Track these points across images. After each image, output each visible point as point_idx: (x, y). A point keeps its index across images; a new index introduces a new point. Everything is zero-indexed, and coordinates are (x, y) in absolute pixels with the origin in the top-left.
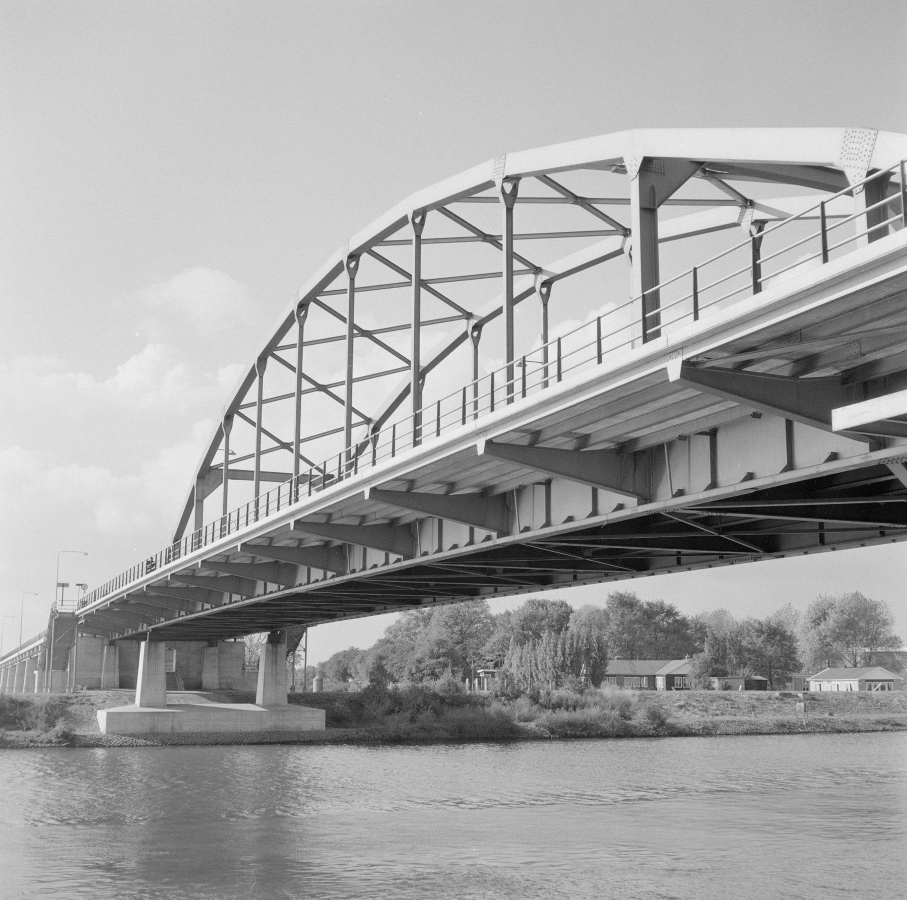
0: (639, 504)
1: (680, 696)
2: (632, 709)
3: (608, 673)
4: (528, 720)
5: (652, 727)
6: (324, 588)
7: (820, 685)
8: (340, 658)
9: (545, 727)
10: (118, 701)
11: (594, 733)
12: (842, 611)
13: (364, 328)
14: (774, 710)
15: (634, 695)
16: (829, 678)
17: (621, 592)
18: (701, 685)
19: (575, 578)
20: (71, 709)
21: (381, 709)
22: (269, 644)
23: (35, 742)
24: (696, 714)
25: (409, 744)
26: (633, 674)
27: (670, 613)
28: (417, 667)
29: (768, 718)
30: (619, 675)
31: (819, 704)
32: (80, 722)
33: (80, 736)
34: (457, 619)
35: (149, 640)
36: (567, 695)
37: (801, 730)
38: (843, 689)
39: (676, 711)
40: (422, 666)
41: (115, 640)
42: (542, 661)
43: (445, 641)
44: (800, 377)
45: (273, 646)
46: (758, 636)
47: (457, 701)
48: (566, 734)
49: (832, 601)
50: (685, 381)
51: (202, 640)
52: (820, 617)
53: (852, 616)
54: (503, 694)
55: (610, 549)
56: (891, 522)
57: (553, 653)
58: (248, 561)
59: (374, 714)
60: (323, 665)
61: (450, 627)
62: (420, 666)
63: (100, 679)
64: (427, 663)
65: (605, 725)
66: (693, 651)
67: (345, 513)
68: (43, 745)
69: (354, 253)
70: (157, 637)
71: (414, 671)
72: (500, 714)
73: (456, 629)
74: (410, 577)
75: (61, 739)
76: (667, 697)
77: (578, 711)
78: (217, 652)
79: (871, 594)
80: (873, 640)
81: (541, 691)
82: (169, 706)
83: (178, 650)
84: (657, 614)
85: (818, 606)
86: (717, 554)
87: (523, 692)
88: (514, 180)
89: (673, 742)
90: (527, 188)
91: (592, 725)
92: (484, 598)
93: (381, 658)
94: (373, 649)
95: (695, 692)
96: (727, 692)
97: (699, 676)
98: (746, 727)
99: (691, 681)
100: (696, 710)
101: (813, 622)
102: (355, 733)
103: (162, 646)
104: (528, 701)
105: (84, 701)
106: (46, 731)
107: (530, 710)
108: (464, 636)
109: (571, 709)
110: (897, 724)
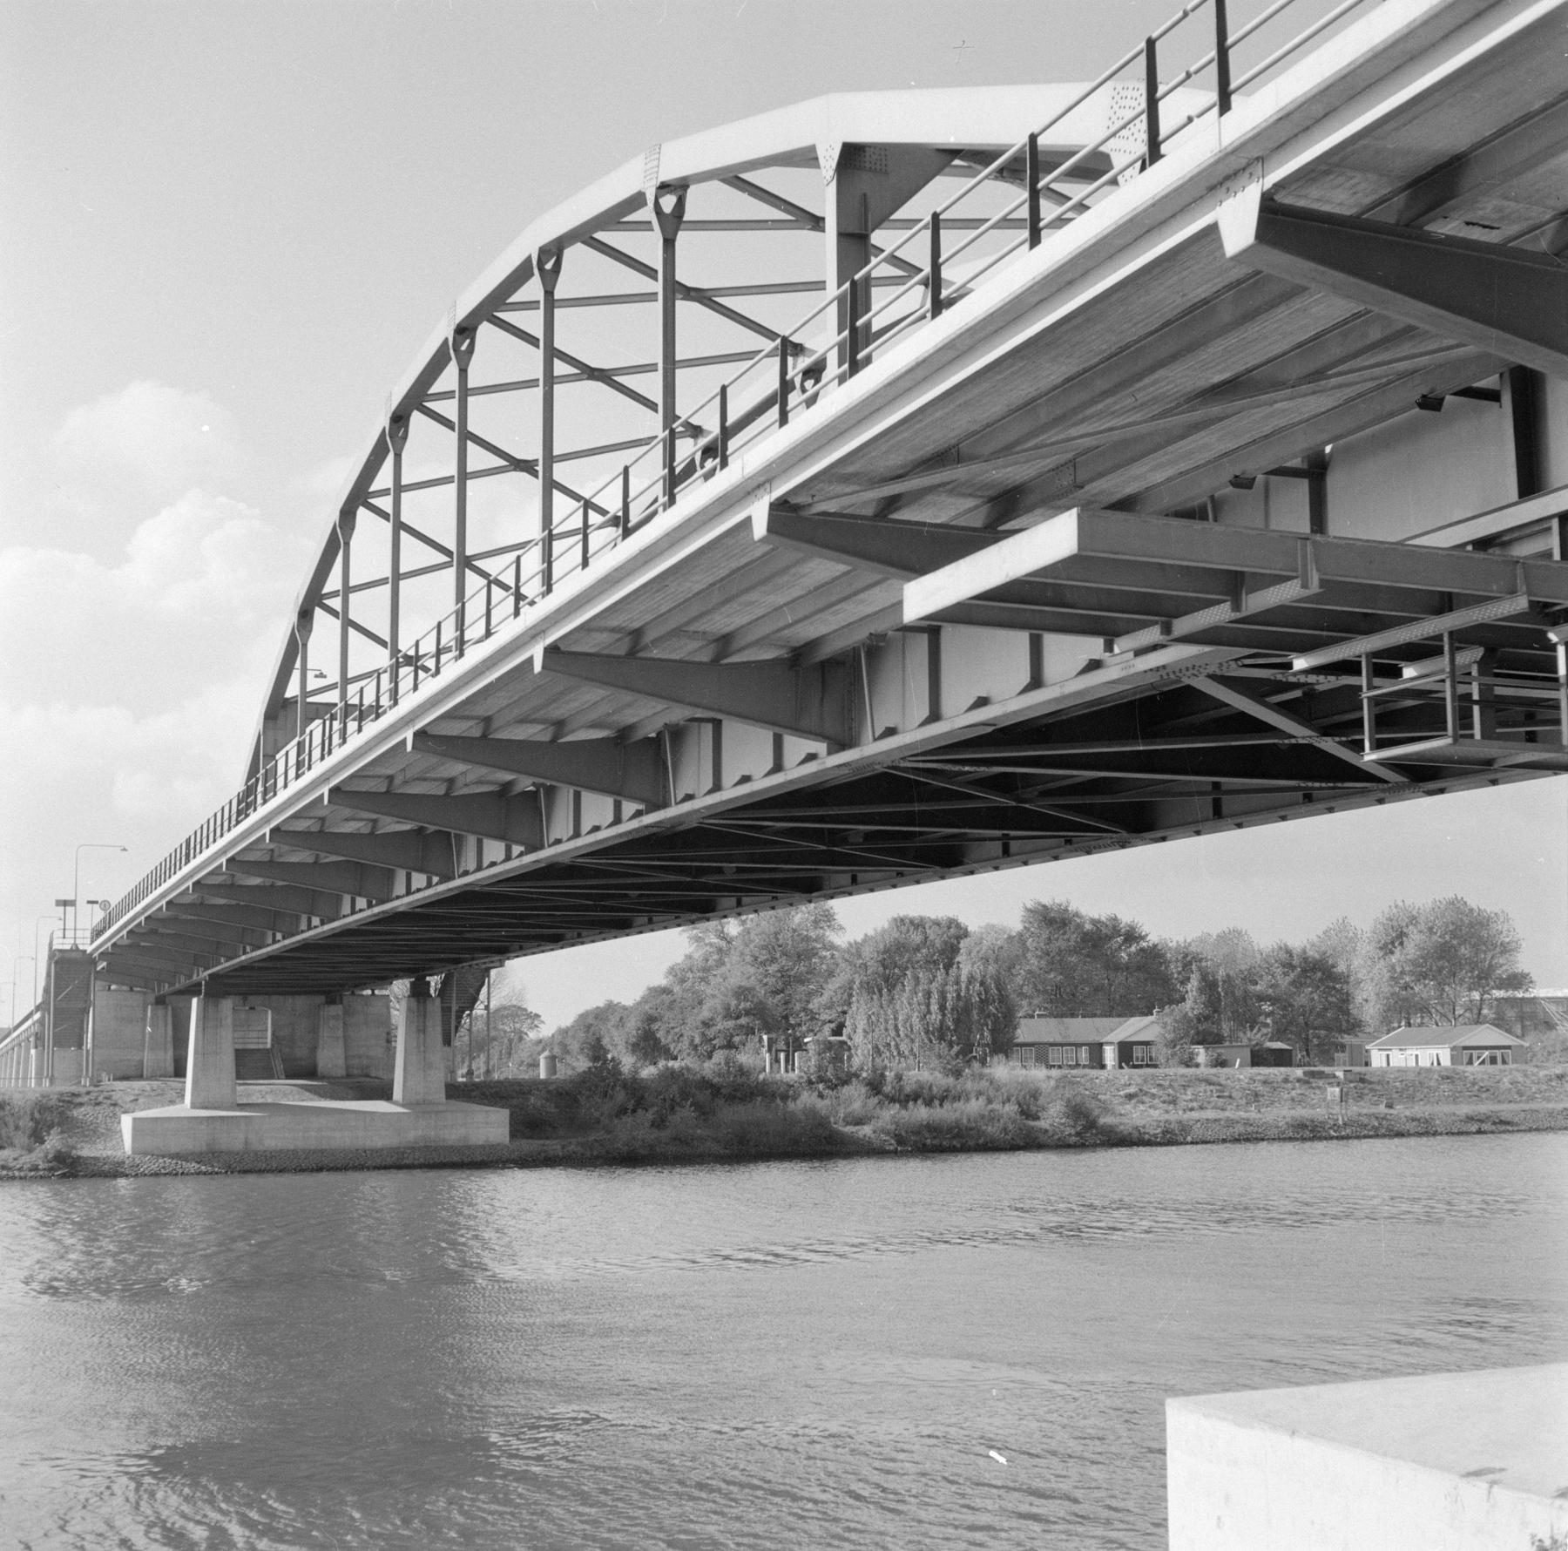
0: (830, 753)
1: (1130, 1078)
2: (1041, 1101)
3: (1020, 1040)
4: (859, 1122)
5: (1073, 1132)
6: (438, 901)
7: (1388, 1056)
8: (590, 1020)
9: (888, 1133)
10: (160, 1099)
11: (971, 1143)
12: (1430, 929)
13: (519, 456)
14: (1293, 1100)
15: (1049, 1078)
16: (1402, 1043)
17: (1046, 901)
18: (1177, 1059)
19: (854, 880)
20: (77, 1113)
21: (608, 1107)
22: (413, 999)
23: (9, 1169)
24: (1156, 1109)
25: (701, 1163)
26: (1064, 1041)
27: (1132, 936)
28: (703, 1034)
29: (1280, 1113)
30: (1039, 1044)
31: (1371, 1090)
32: (90, 1132)
33: (88, 1158)
34: (773, 949)
35: (206, 994)
36: (931, 1078)
37: (1333, 1133)
38: (1425, 1063)
39: (1122, 1104)
40: (711, 1033)
41: (164, 996)
42: (906, 1021)
43: (750, 990)
44: (1000, 528)
45: (419, 1002)
46: (1285, 974)
47: (743, 1089)
48: (924, 1145)
49: (1414, 913)
50: (777, 539)
51: (319, 993)
52: (1394, 939)
53: (1447, 937)
54: (821, 1080)
55: (878, 831)
56: (1301, 779)
57: (923, 1007)
58: (311, 860)
59: (597, 1114)
60: (564, 1032)
61: (763, 964)
62: (707, 1032)
63: (141, 1062)
64: (720, 1027)
65: (992, 1130)
66: (1171, 997)
67: (409, 774)
68: (22, 1174)
69: (464, 325)
70: (217, 989)
71: (697, 1040)
72: (812, 1113)
73: (773, 968)
74: (540, 883)
75: (54, 1164)
76: (1108, 1081)
77: (947, 1105)
78: (340, 1013)
79: (1480, 900)
80: (1483, 977)
81: (887, 1073)
82: (242, 1107)
83: (276, 1011)
84: (1109, 938)
87: (856, 1075)
88: (679, 187)
89: (1364, 1146)
90: (702, 202)
91: (971, 1129)
92: (725, 917)
93: (651, 1019)
94: (639, 1004)
95: (1167, 1071)
96: (1218, 1070)
97: (1172, 1044)
98: (1240, 1129)
99: (1160, 1052)
100: (1156, 1101)
101: (1381, 948)
102: (559, 1147)
103: (227, 1005)
104: (864, 1090)
105: (100, 1099)
106: (30, 1151)
107: (864, 1105)
108: (787, 980)
109: (937, 1102)
110: (1502, 1122)
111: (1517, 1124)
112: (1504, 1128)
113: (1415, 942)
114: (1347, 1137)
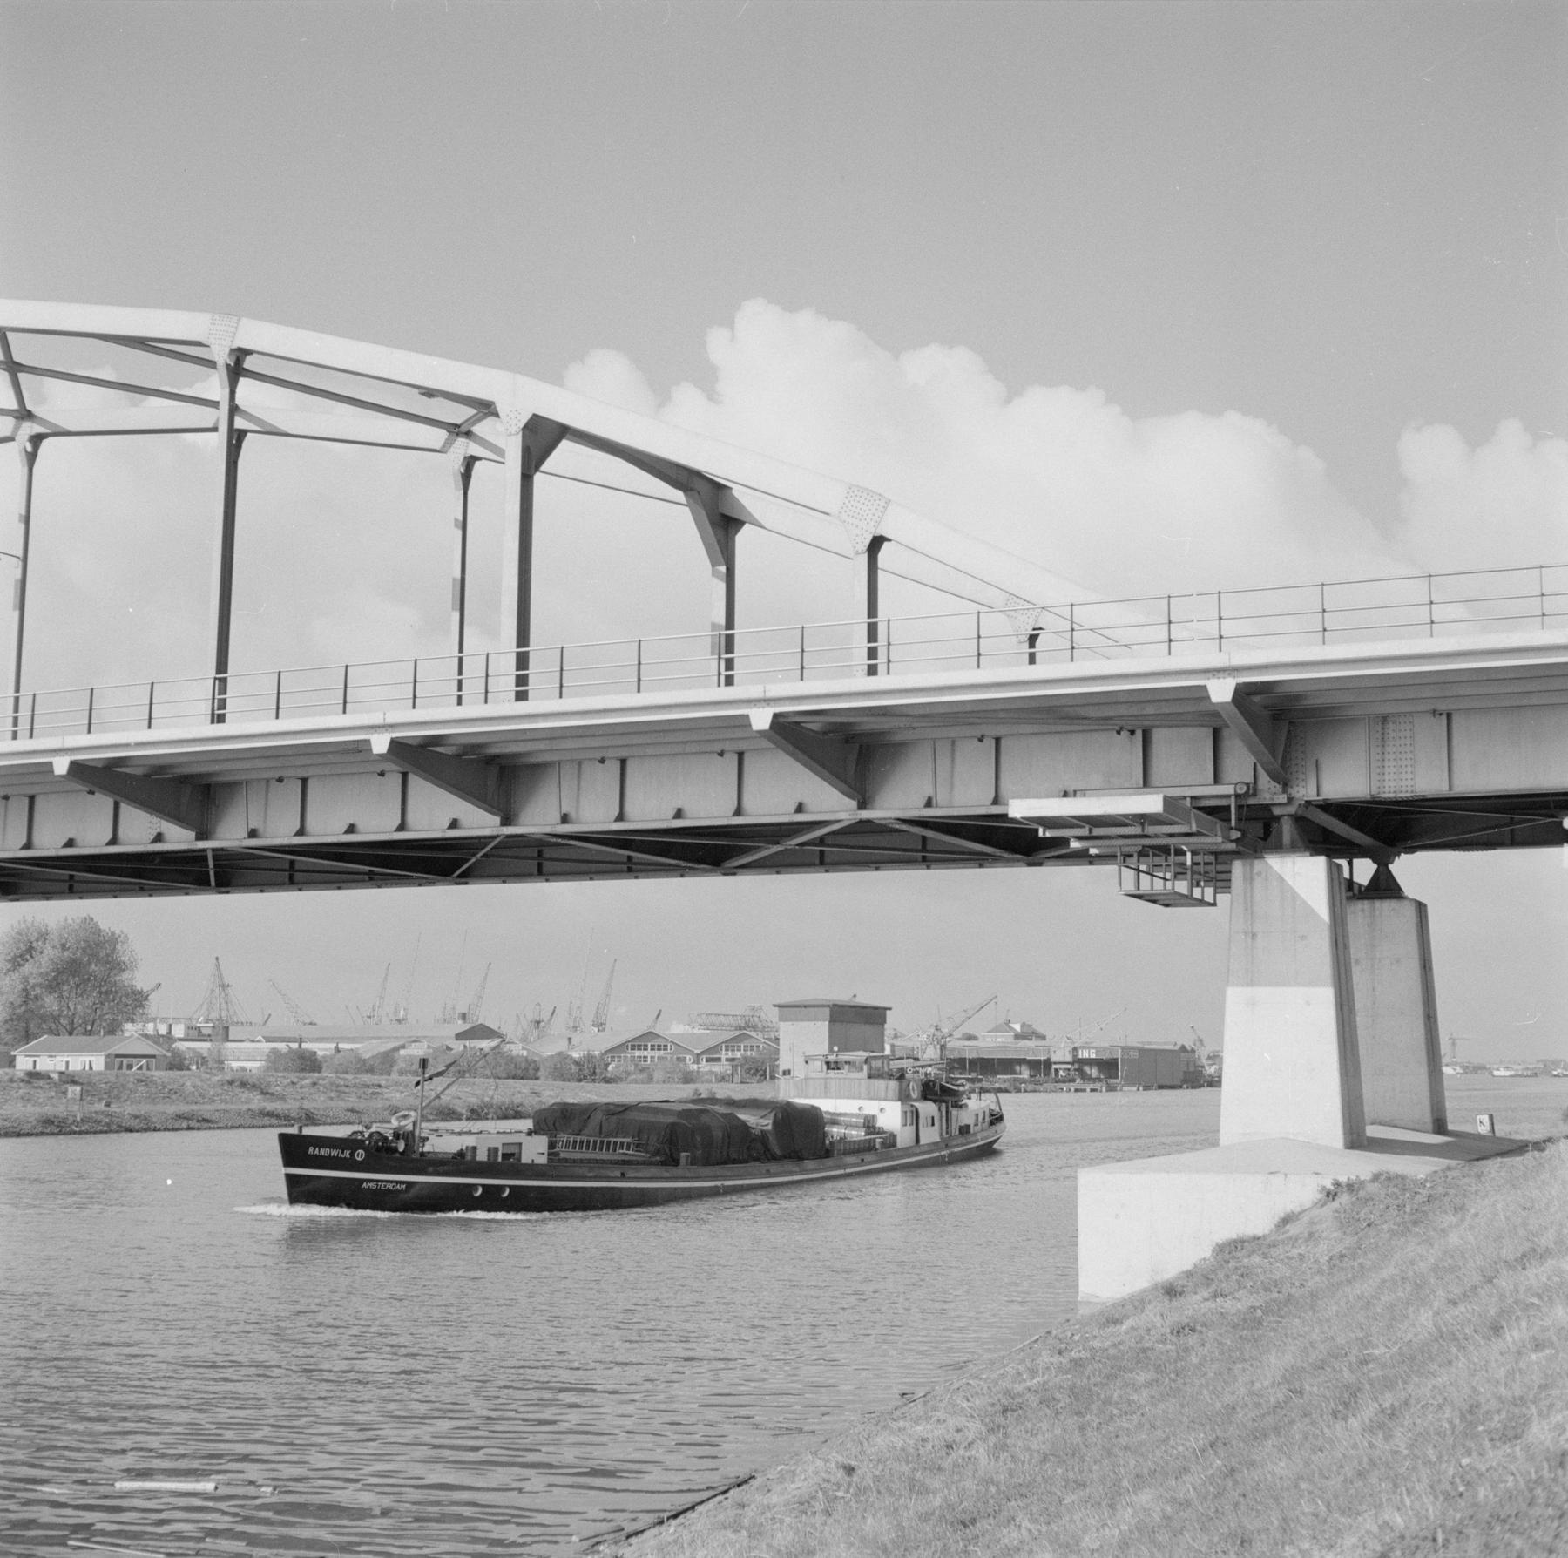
7: (35, 1062)
14: (22, 1098)
16: (51, 1051)
37: (77, 1129)
85: (21, 934)
86: (135, 884)
101: (9, 961)
111: (217, 1122)
112: (206, 1125)
113: (48, 956)
114: (87, 1132)
